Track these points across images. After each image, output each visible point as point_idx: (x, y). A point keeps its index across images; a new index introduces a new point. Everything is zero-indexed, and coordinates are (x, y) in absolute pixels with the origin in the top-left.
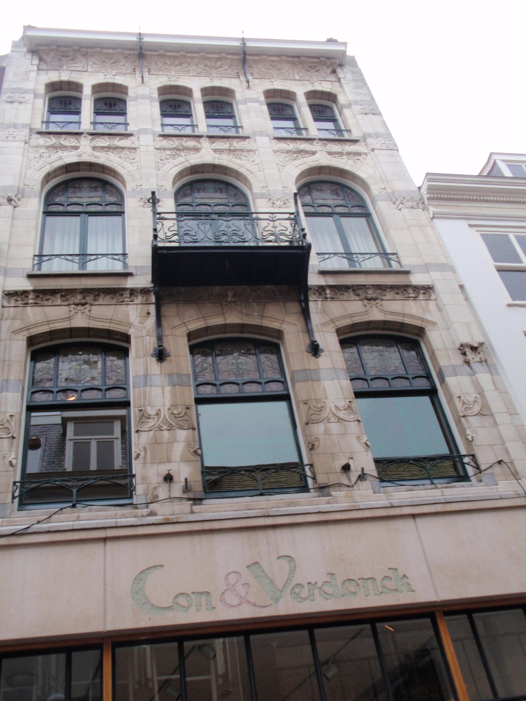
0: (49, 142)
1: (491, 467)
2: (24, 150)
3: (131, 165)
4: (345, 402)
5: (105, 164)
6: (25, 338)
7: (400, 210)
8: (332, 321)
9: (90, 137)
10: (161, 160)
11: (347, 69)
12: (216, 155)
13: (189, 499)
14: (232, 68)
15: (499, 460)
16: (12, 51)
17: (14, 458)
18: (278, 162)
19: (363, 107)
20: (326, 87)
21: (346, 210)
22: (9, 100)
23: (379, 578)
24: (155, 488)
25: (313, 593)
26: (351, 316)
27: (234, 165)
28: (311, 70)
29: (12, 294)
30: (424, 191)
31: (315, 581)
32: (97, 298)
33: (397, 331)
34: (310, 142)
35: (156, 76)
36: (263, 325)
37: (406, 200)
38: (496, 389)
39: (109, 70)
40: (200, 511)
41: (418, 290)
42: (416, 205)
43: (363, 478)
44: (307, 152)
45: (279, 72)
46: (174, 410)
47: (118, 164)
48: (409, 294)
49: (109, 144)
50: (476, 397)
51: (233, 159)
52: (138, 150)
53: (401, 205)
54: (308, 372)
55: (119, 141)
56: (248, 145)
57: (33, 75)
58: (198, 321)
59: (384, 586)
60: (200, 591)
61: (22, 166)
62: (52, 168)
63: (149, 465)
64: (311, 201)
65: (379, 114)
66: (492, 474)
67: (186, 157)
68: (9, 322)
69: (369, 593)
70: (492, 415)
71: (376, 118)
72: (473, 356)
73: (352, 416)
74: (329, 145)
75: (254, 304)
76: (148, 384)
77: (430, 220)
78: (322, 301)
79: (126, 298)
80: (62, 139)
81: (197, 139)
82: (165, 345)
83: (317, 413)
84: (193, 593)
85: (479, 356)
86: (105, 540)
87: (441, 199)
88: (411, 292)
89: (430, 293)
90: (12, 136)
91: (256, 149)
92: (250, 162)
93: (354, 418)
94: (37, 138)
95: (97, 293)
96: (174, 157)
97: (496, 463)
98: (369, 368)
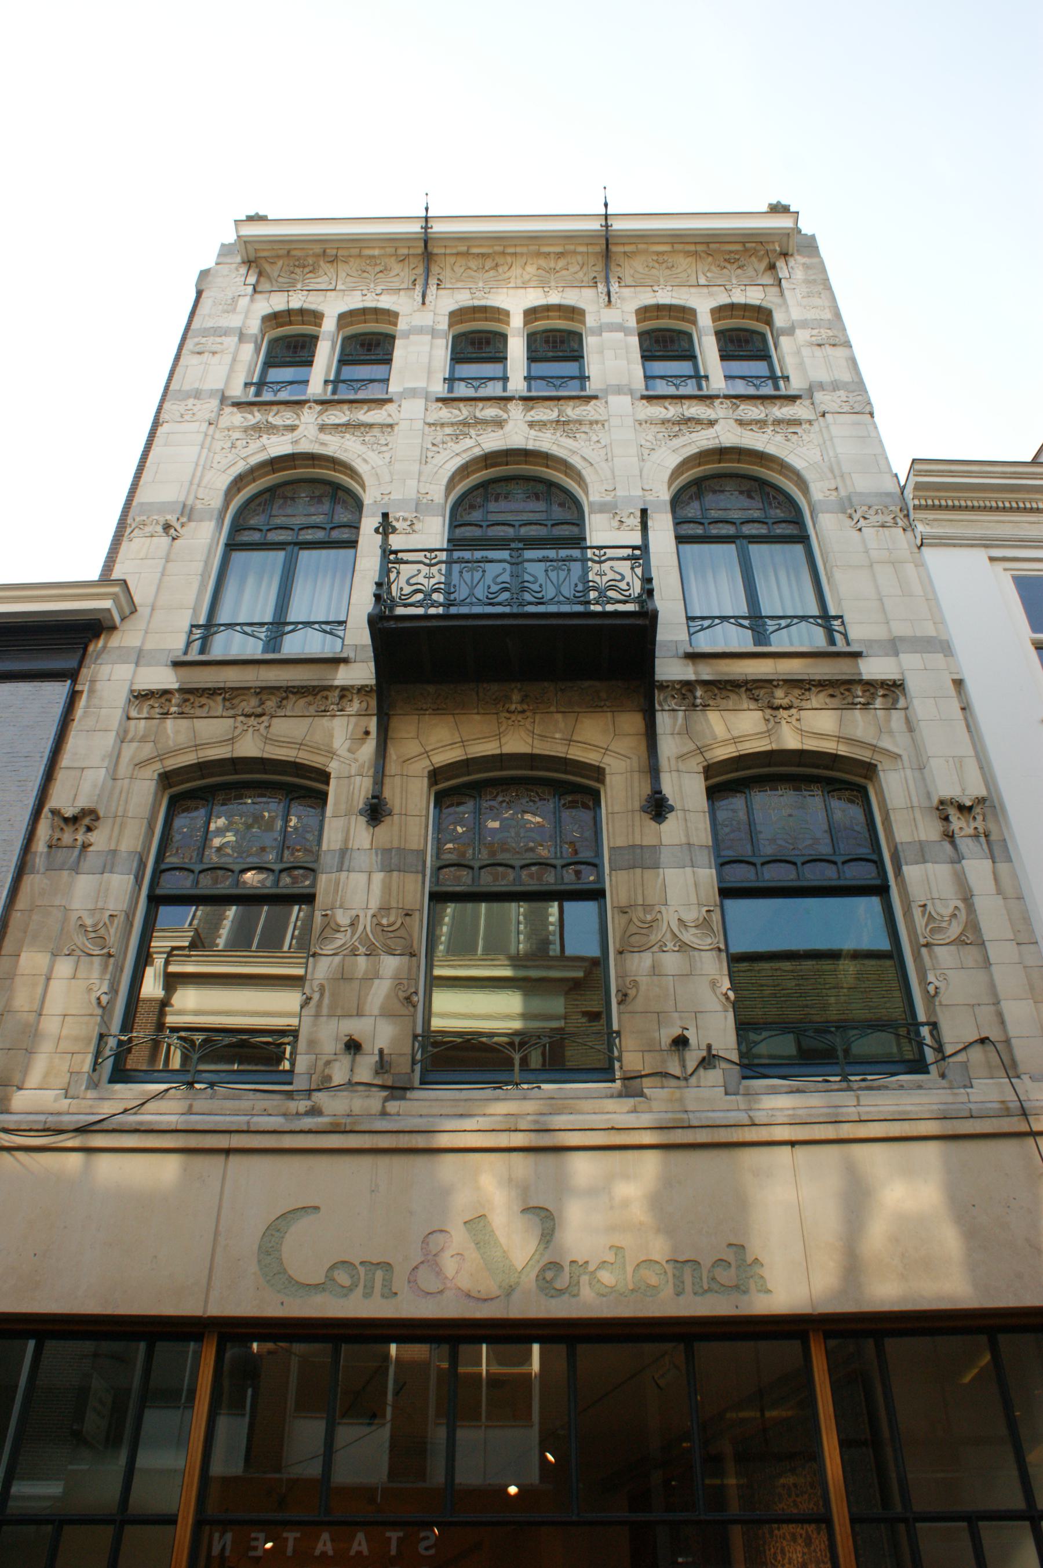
0: (250, 420)
1: (965, 1048)
2: (206, 435)
3: (381, 455)
4: (699, 911)
5: (336, 455)
6: (156, 776)
7: (860, 530)
8: (698, 751)
9: (318, 408)
10: (434, 445)
11: (798, 262)
12: (533, 432)
13: (383, 1087)
14: (585, 269)
15: (983, 1035)
16: (217, 264)
17: (106, 993)
18: (643, 442)
19: (815, 332)
20: (753, 296)
21: (763, 530)
22: (197, 349)
23: (707, 1262)
24: (328, 1063)
25: (579, 1282)
26: (736, 740)
27: (561, 451)
28: (728, 265)
29: (146, 695)
30: (909, 493)
31: (586, 1260)
32: (285, 702)
33: (826, 768)
34: (708, 402)
35: (451, 291)
36: (569, 756)
37: (872, 511)
38: (999, 891)
39: (372, 286)
40: (399, 1112)
41: (872, 690)
42: (892, 521)
43: (709, 1064)
44: (698, 421)
45: (670, 273)
46: (383, 917)
47: (356, 455)
48: (854, 697)
49: (348, 418)
50: (956, 907)
51: (560, 439)
52: (396, 428)
53: (862, 520)
54: (639, 851)
55: (366, 413)
56: (593, 412)
57: (244, 302)
58: (452, 749)
59: (713, 1279)
60: (375, 1262)
61: (197, 465)
62: (248, 466)
63: (323, 1019)
64: (699, 513)
65: (847, 344)
66: (965, 1065)
67: (478, 438)
68: (135, 745)
69: (683, 1289)
70: (983, 943)
71: (840, 352)
72: (962, 823)
73: (709, 941)
74: (742, 407)
75: (559, 717)
76: (345, 867)
77: (916, 550)
78: (685, 711)
79: (332, 704)
80: (272, 414)
81: (502, 403)
82: (387, 794)
83: (644, 931)
84: (362, 1263)
85: (973, 825)
86: (228, 1152)
88: (860, 693)
89: (898, 695)
90: (190, 412)
91: (605, 418)
92: (592, 443)
93: (710, 945)
94: (232, 413)
95: (284, 695)
96: (456, 438)
97: (976, 1041)
98: (762, 842)
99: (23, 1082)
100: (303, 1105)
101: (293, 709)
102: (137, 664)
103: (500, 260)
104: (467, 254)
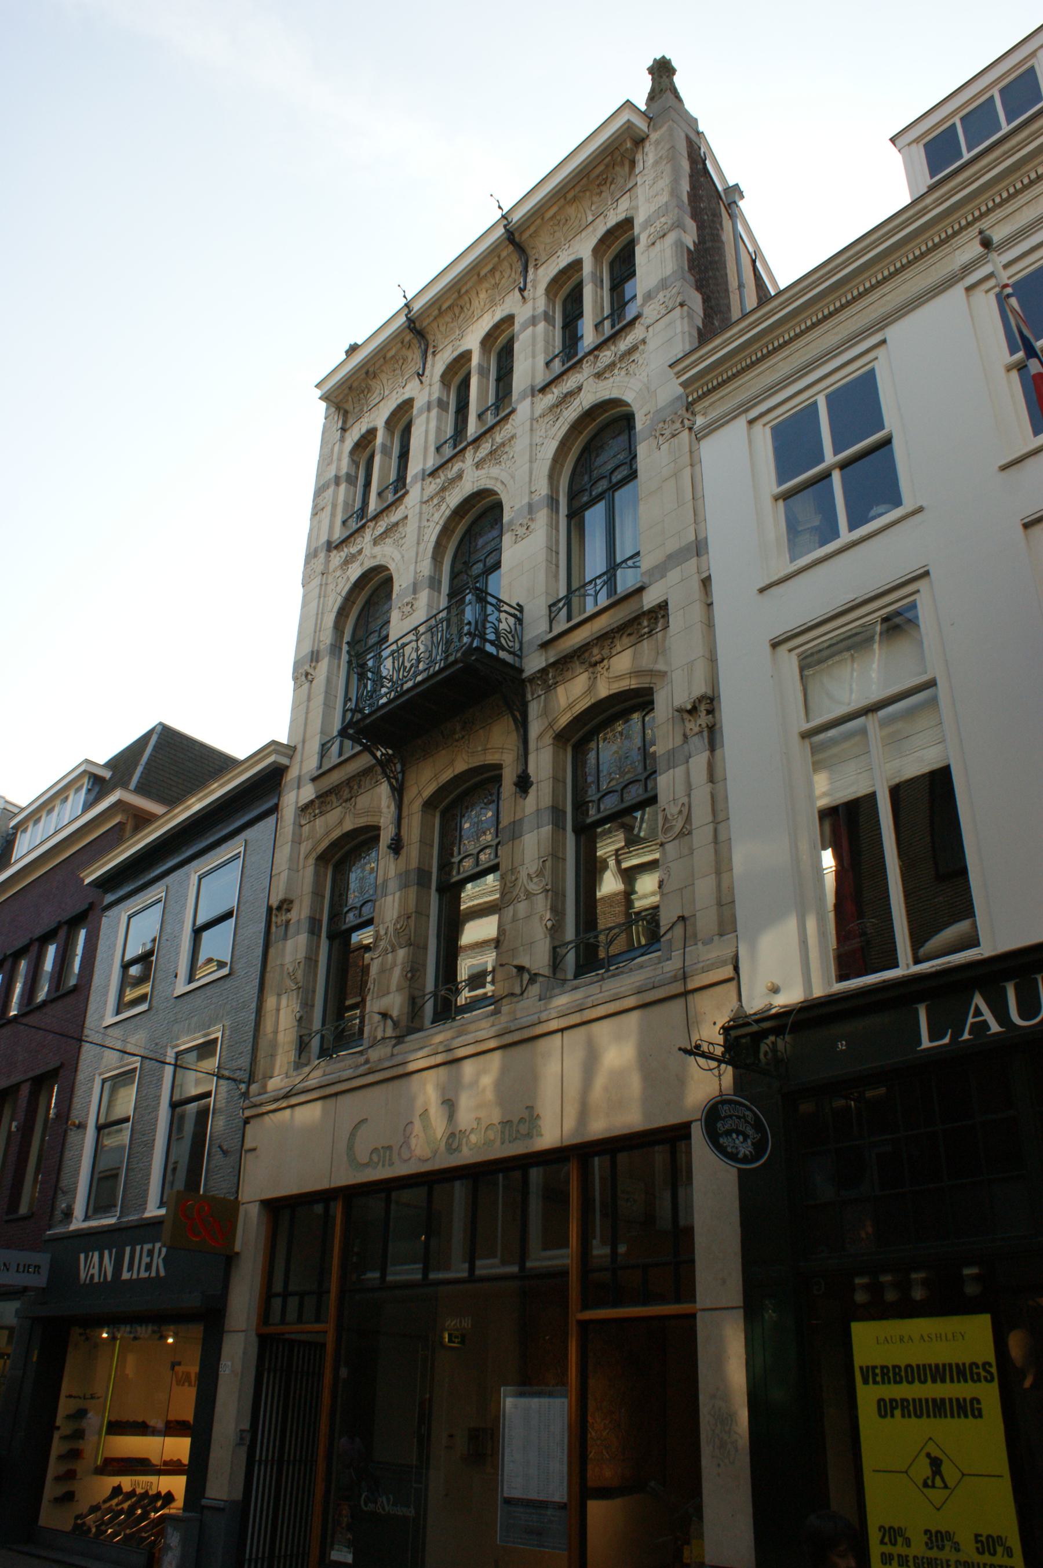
23: (516, 1121)
84: (382, 1147)
86: (336, 1094)
87: (710, 392)
99: (273, 1073)
100: (362, 1059)
101: (365, 787)
102: (299, 788)
103: (461, 302)
104: (441, 313)
